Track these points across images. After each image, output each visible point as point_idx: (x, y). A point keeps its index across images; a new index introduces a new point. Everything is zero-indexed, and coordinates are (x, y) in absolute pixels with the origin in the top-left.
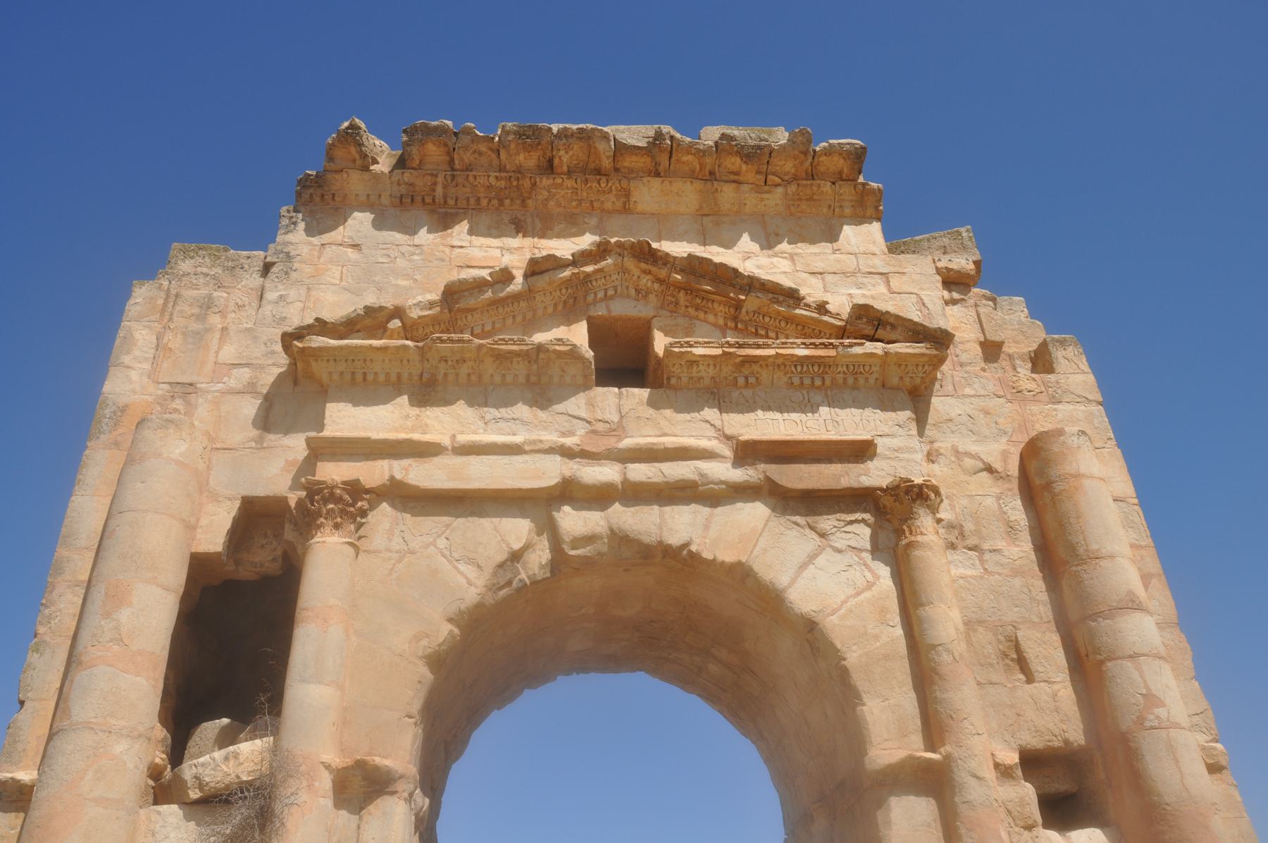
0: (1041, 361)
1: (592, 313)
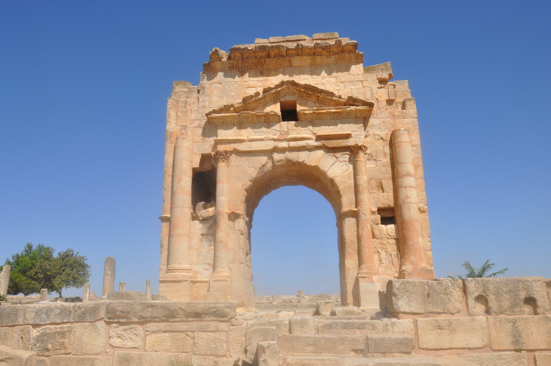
1: (281, 100)
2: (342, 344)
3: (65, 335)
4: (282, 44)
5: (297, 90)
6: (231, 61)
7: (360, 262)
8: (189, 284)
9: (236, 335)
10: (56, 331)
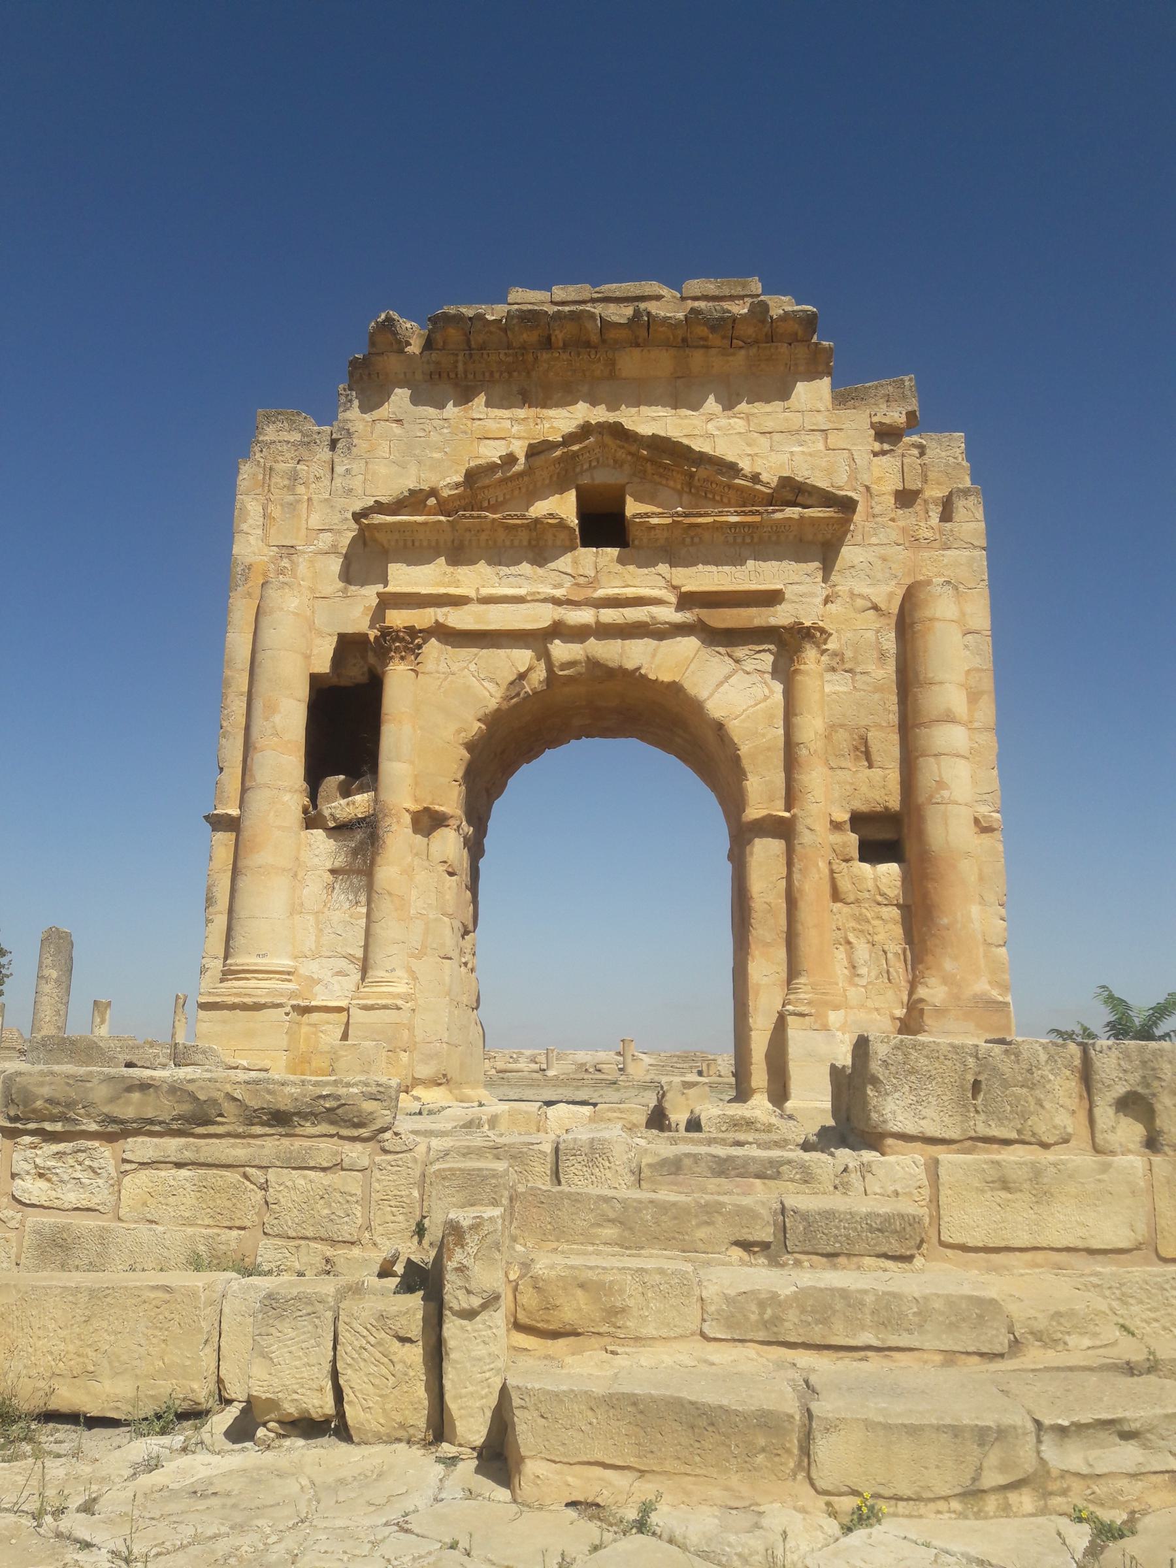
1: (580, 482)
2: (708, 1223)
4: (588, 307)
5: (630, 453)
6: (435, 356)
7: (793, 971)
8: (287, 1014)
9: (394, 1181)
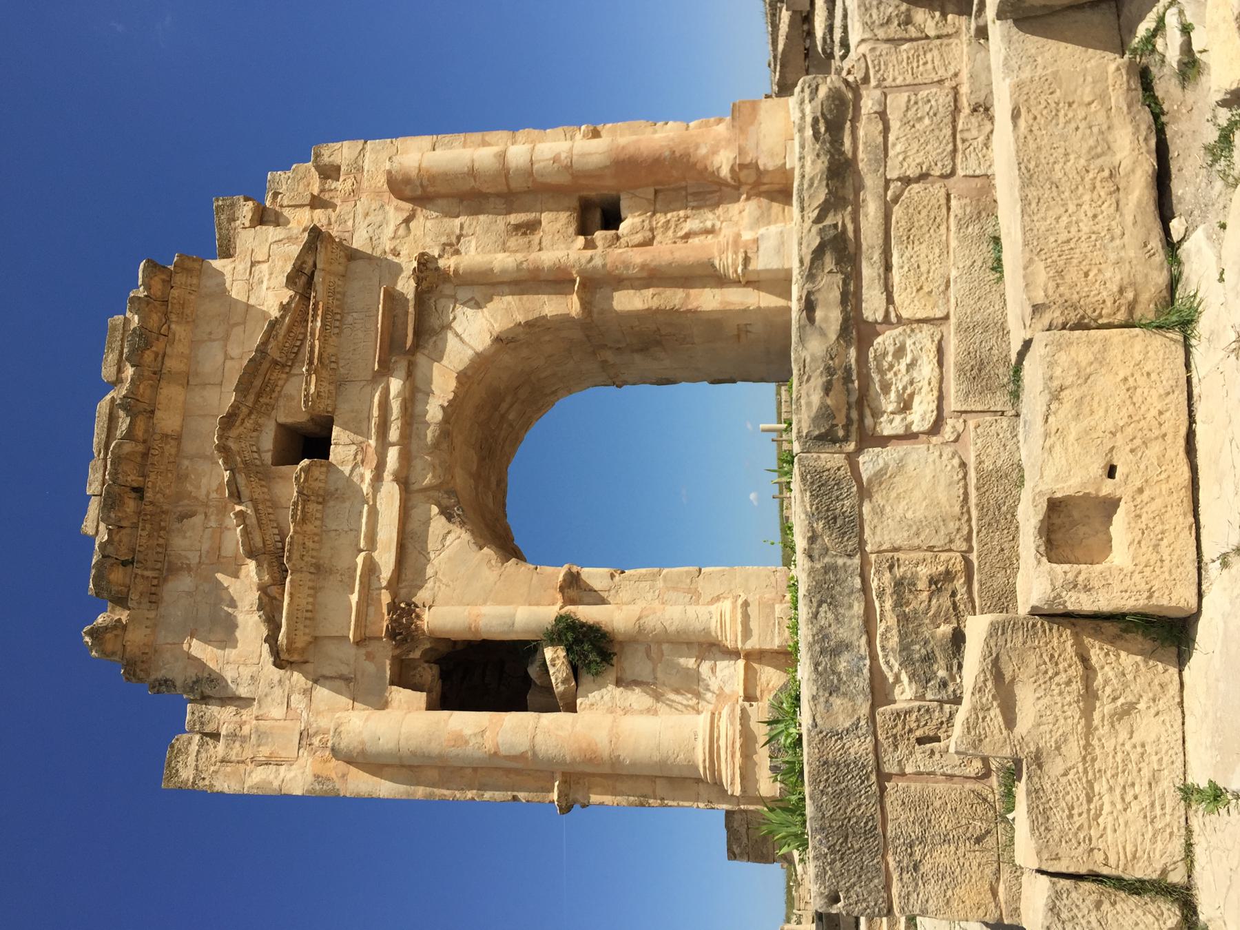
0: (329, 173)
1: (270, 462)
3: (903, 578)
5: (250, 413)
6: (134, 596)
10: (893, 610)
